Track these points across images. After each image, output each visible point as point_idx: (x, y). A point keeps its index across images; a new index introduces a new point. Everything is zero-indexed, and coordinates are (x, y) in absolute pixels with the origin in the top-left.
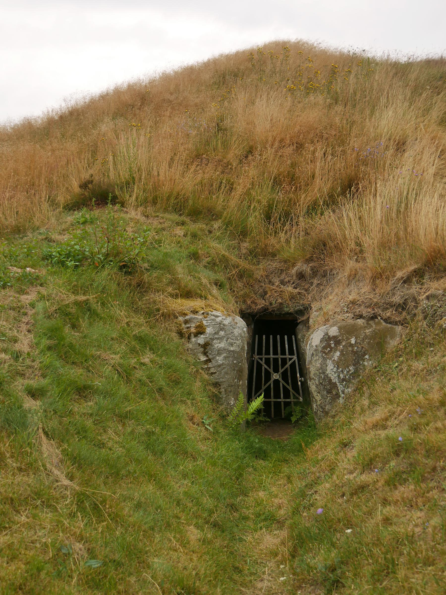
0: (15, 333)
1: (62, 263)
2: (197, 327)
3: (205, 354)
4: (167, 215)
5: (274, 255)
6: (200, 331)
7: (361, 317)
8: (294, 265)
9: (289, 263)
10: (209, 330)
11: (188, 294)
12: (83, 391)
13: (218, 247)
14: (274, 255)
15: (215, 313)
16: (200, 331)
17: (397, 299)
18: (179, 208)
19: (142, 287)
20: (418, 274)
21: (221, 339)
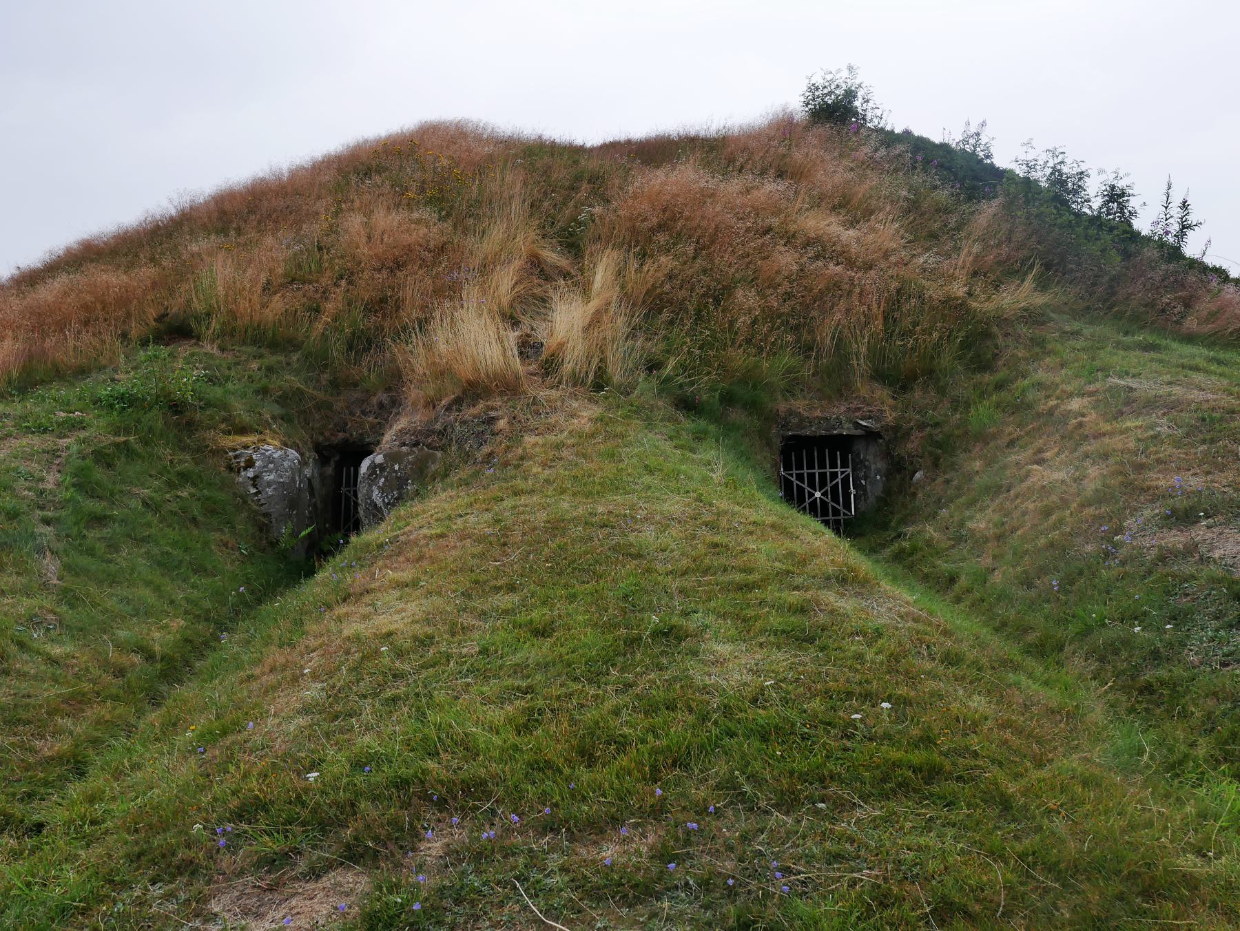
0: (44, 473)
1: (111, 406)
2: (246, 461)
3: (255, 486)
4: (244, 348)
5: (355, 385)
6: (250, 463)
7: (404, 444)
8: (375, 394)
9: (368, 393)
10: (257, 464)
11: (243, 430)
12: (99, 520)
13: (290, 380)
14: (355, 385)
15: (266, 447)
16: (250, 463)
17: (438, 426)
18: (255, 341)
19: (191, 426)
20: (458, 401)
21: (270, 471)
